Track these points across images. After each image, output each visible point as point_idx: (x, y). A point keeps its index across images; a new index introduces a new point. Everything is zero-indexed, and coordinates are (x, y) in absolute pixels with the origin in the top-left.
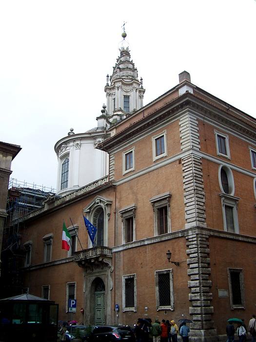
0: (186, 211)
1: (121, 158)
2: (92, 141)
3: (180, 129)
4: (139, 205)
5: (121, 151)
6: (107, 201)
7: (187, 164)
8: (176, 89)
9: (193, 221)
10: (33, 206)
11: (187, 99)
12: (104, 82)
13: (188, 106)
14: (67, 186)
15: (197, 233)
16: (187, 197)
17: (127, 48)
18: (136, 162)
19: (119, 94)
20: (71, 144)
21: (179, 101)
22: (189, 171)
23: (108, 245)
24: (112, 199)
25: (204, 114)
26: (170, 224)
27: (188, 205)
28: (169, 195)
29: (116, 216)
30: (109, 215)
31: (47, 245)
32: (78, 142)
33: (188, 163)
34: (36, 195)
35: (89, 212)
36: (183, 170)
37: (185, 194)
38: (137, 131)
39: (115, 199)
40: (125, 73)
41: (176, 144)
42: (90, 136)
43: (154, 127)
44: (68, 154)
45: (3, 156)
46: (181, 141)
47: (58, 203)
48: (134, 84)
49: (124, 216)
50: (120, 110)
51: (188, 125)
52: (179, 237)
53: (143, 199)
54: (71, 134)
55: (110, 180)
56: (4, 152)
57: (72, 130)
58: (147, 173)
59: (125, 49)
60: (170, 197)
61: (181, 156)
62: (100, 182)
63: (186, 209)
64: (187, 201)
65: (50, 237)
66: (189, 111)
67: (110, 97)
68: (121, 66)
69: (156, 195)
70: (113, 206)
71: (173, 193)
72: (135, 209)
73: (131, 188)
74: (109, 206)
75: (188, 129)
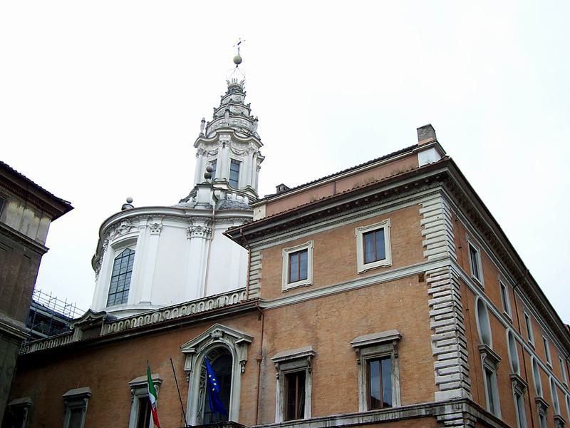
0: (437, 369)
1: (280, 260)
2: (186, 226)
3: (423, 222)
4: (321, 350)
5: (281, 250)
6: (246, 336)
7: (439, 283)
8: (412, 152)
9: (454, 388)
10: (34, 332)
11: (446, 169)
12: (196, 131)
13: (441, 183)
14: (124, 300)
15: (464, 410)
16: (439, 343)
17: (243, 82)
18: (315, 270)
19: (224, 156)
20: (143, 223)
21: (430, 172)
22: (444, 299)
23: (240, 417)
24: (250, 333)
25: (457, 202)
26: (398, 390)
27: (440, 357)
28: (399, 335)
29: (262, 368)
30: (244, 363)
31: (72, 410)
32: (159, 222)
33: (442, 282)
34: (38, 311)
35: (193, 354)
36: (431, 294)
37: (434, 336)
38: (325, 214)
39: (260, 334)
40: (237, 121)
41: (414, 246)
42: (184, 215)
43: (363, 212)
44: (133, 241)
45: (36, 215)
46: (425, 242)
47: (117, 328)
48: (252, 144)
49: (283, 367)
50: (225, 183)
51: (440, 216)
52: (420, 417)
53: (332, 340)
54: (128, 207)
55: (250, 297)
56: (38, 207)
57: (130, 202)
58: (345, 291)
59: (239, 83)
60: (399, 340)
61: (425, 268)
62: (156, 315)
63: (437, 364)
64: (440, 350)
65: (85, 395)
66: (441, 192)
67: (205, 158)
68: (232, 109)
69: (364, 334)
70: (256, 347)
71: (406, 332)
72: (310, 358)
73: (302, 317)
74: (245, 347)
75: (441, 222)
